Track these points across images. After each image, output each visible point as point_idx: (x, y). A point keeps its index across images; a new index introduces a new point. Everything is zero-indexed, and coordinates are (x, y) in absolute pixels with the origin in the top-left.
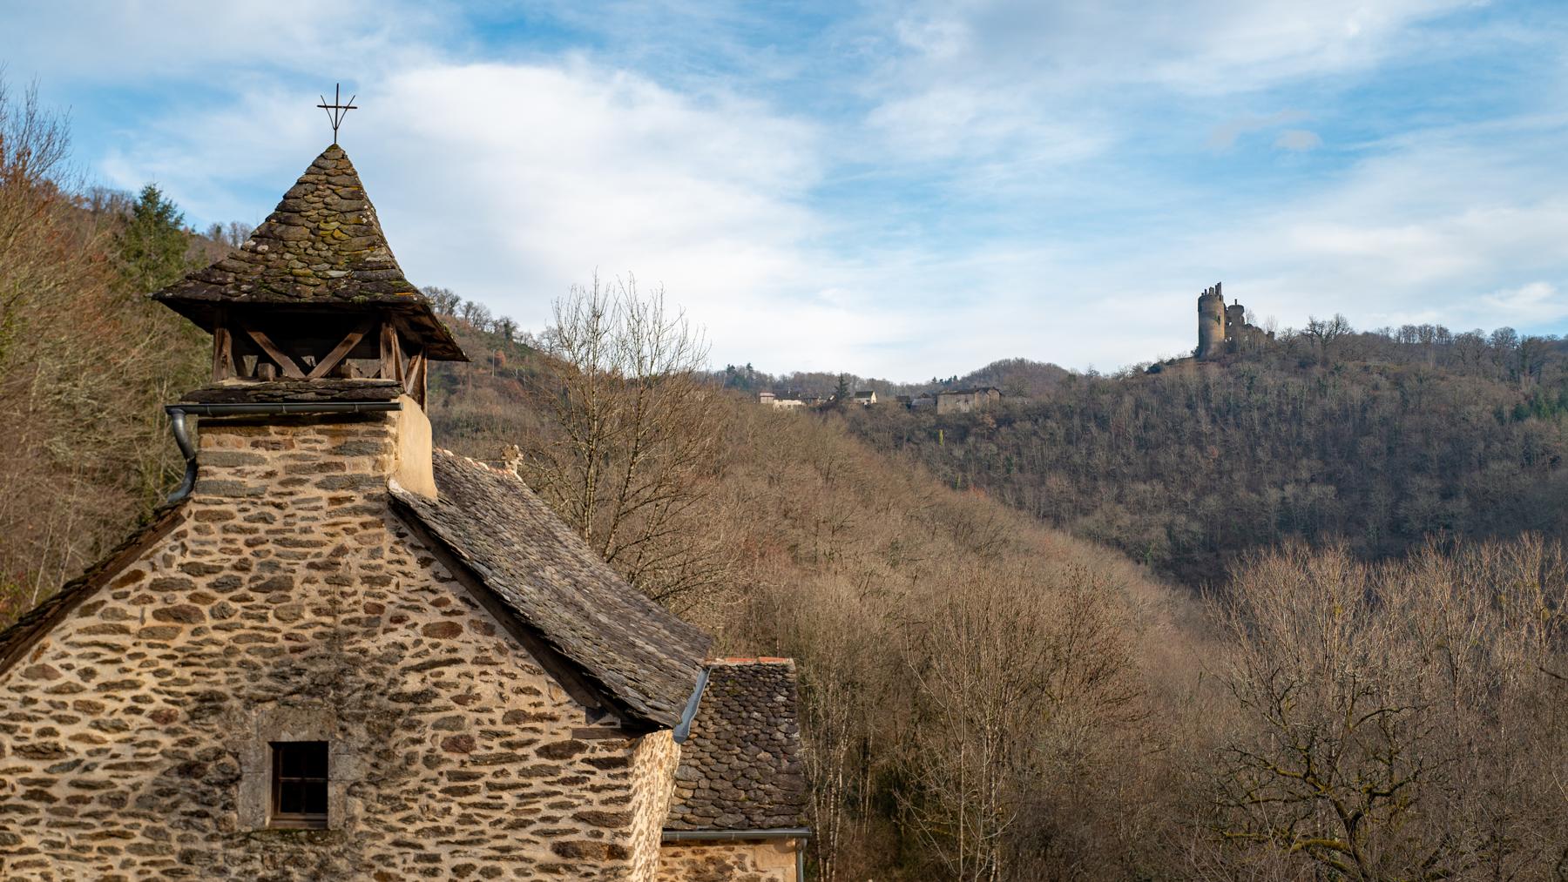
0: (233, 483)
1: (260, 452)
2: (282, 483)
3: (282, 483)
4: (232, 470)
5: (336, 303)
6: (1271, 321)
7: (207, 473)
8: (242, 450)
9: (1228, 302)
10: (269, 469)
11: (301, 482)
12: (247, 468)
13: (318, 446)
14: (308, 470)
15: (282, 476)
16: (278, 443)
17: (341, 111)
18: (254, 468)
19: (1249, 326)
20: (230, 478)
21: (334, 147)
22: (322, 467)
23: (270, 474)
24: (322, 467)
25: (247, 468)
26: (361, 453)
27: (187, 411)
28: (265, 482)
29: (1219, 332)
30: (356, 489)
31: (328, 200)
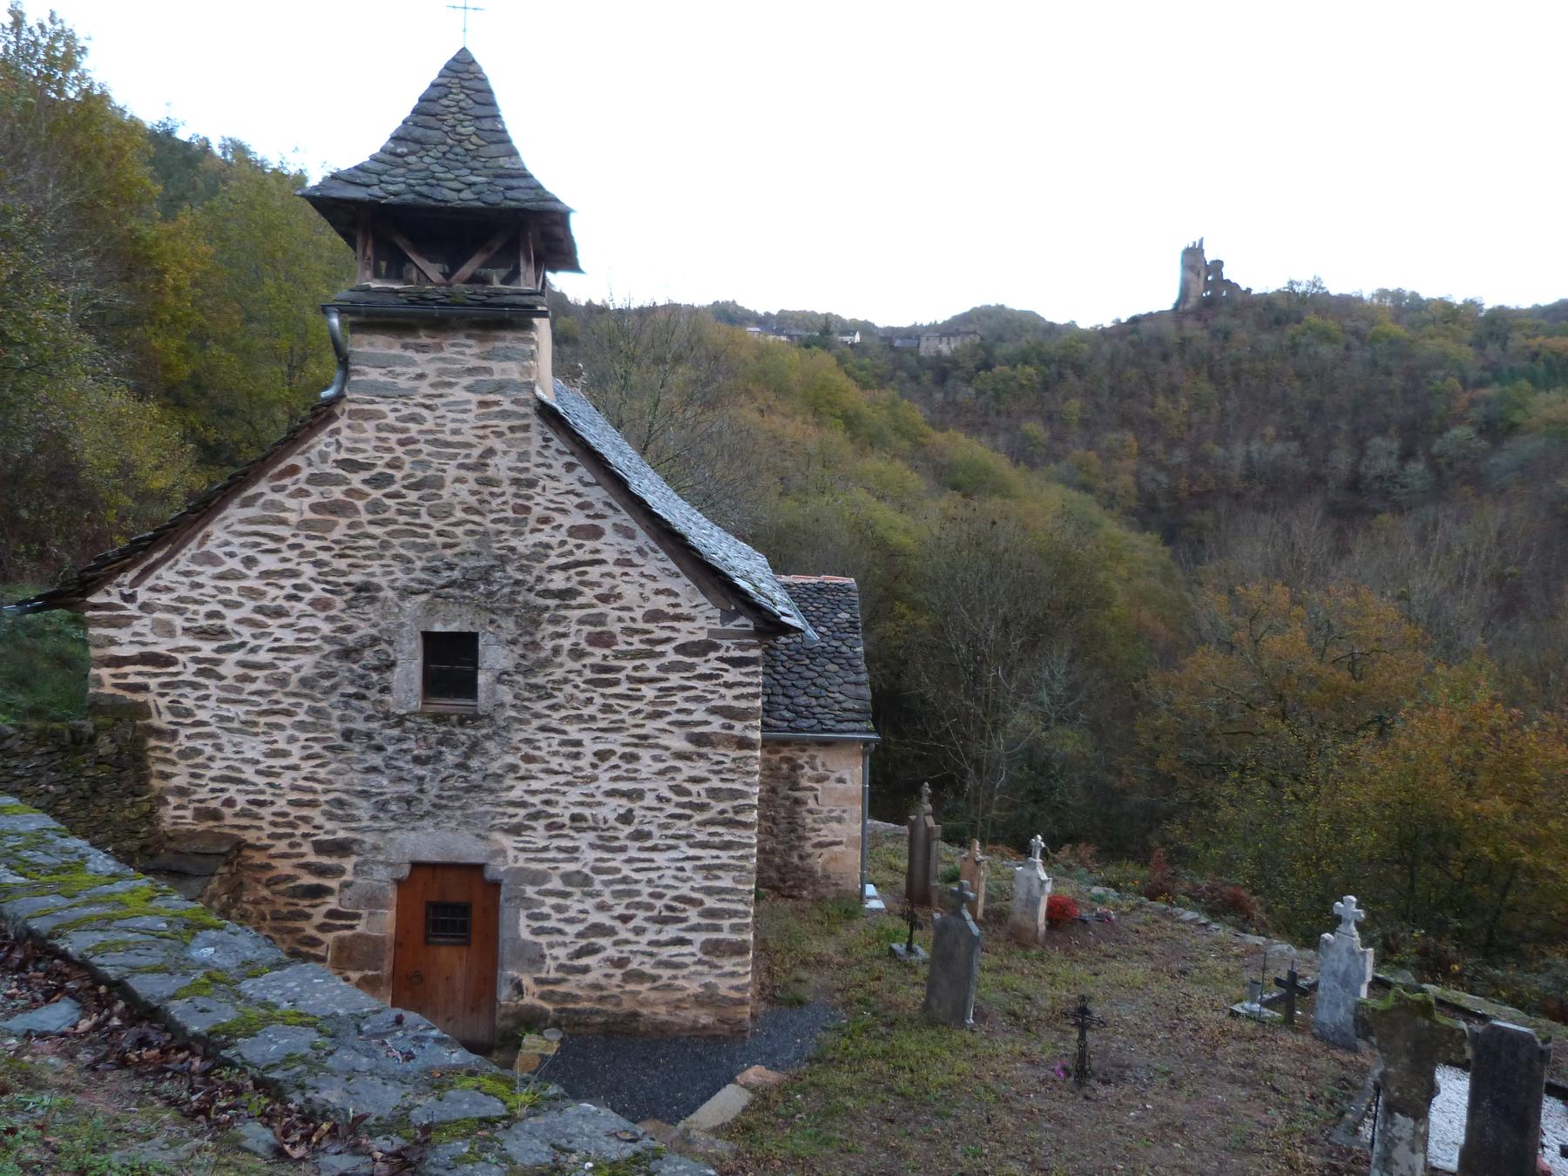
0: (385, 383)
1: (410, 353)
2: (432, 385)
3: (432, 385)
7: (358, 372)
8: (393, 352)
9: (1209, 257)
10: (419, 371)
11: (450, 385)
12: (398, 369)
13: (467, 351)
14: (458, 374)
15: (432, 378)
20: (382, 379)
22: (471, 371)
23: (421, 376)
24: (471, 371)
25: (398, 369)
26: (507, 358)
28: (415, 383)
31: (462, 104)
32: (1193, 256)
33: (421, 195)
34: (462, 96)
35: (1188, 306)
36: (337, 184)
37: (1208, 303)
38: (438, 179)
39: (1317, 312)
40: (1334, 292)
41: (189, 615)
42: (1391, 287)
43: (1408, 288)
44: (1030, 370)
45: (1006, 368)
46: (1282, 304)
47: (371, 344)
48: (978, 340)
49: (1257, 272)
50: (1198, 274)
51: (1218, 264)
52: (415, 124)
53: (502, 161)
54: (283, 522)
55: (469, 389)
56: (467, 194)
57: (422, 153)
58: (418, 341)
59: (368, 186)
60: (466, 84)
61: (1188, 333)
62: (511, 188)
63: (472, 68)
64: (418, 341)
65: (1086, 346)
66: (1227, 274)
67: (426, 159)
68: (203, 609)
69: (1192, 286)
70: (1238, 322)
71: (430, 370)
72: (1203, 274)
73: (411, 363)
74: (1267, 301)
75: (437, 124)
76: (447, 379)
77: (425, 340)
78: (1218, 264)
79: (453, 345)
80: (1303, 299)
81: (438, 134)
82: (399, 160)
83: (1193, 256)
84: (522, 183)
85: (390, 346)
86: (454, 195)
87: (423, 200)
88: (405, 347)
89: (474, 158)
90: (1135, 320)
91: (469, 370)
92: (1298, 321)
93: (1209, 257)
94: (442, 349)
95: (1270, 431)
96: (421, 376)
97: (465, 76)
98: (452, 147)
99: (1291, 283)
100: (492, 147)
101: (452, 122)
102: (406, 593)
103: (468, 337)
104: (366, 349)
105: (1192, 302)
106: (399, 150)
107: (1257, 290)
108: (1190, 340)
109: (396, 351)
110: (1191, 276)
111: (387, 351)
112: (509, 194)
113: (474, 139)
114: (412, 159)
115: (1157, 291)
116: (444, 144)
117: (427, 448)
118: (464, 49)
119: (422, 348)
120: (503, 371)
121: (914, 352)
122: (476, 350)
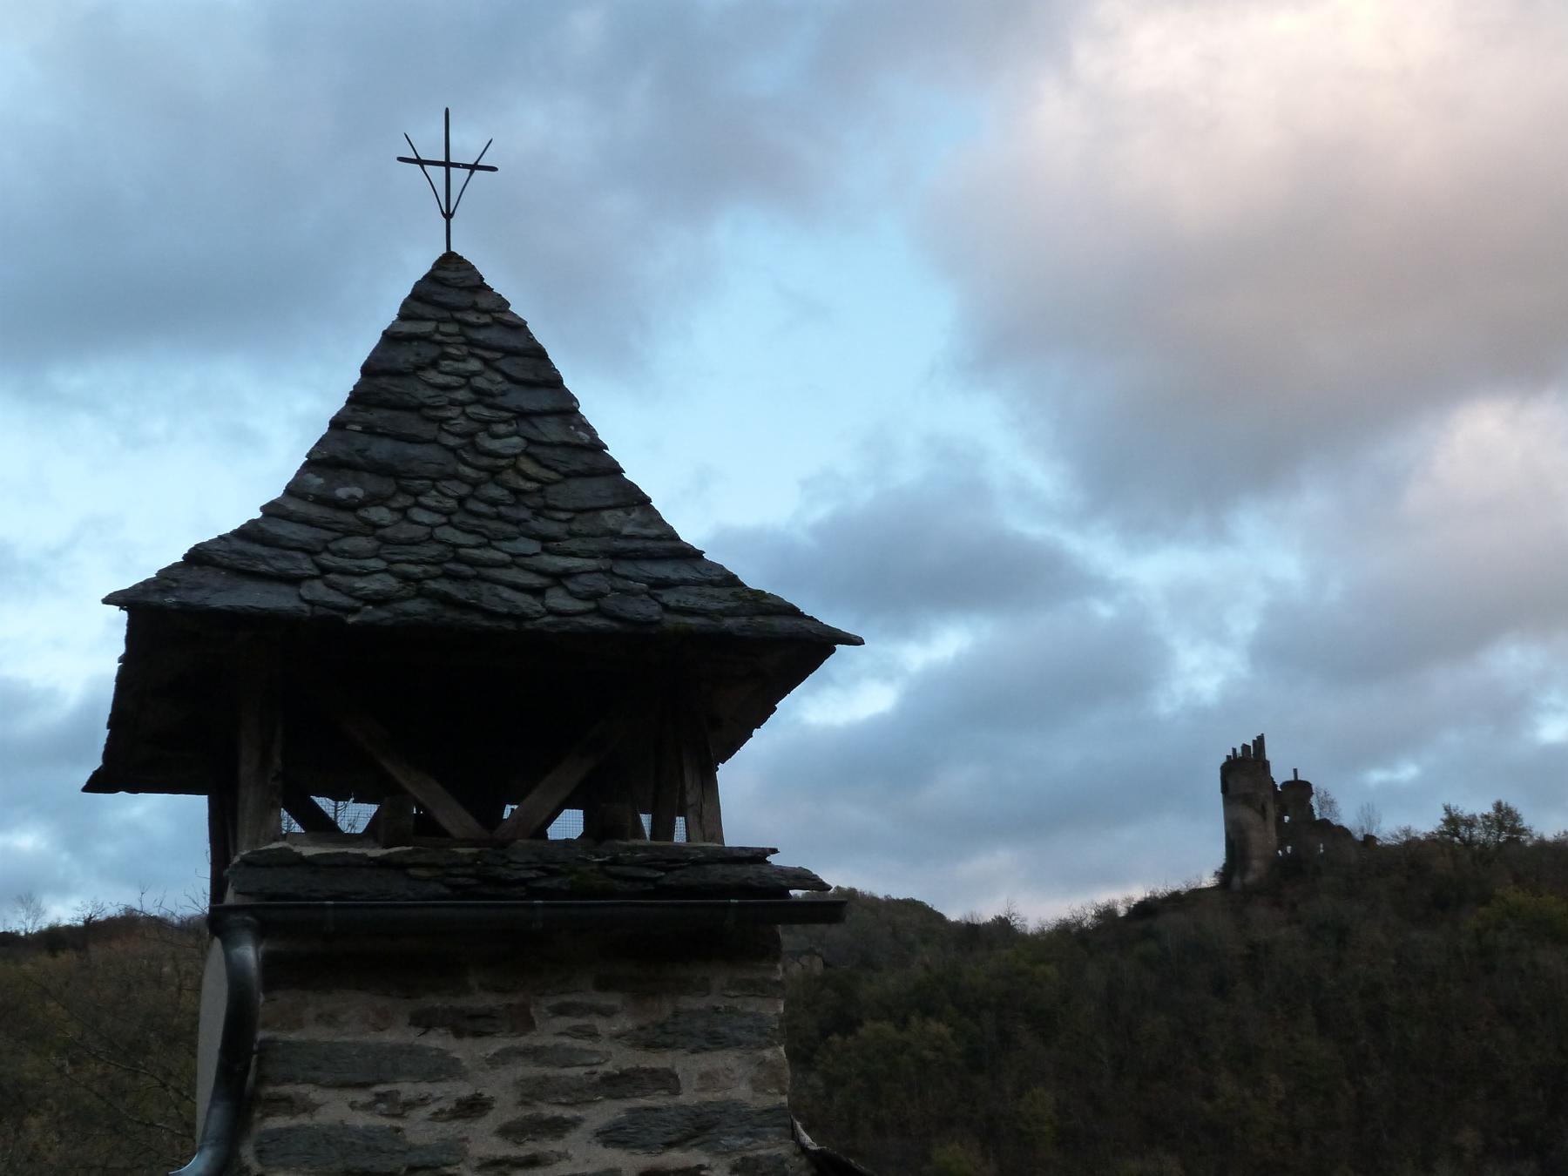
0: (368, 1134)
1: (436, 1040)
2: (505, 1132)
3: (505, 1132)
4: (363, 1097)
5: (596, 633)
6: (1368, 813)
7: (289, 1105)
8: (390, 1037)
9: (1280, 774)
10: (465, 1091)
11: (558, 1127)
12: (407, 1089)
13: (601, 1024)
14: (582, 1094)
15: (507, 1110)
16: (489, 1015)
17: (438, 173)
18: (425, 1088)
19: (1325, 823)
20: (361, 1120)
21: (450, 260)
22: (616, 1084)
23: (474, 1107)
24: (616, 1084)
25: (407, 1089)
26: (716, 1041)
27: (263, 931)
28: (454, 1128)
29: (1264, 840)
30: (710, 1147)
31: (479, 382)
33: (446, 600)
34: (474, 365)
35: (1251, 878)
36: (214, 578)
38: (472, 563)
39: (1518, 880)
40: (1549, 836)
44: (937, 1027)
45: (887, 1028)
47: (329, 1019)
48: (818, 967)
50: (1263, 812)
52: (369, 430)
53: (610, 519)
55: (612, 1137)
56: (558, 599)
57: (402, 501)
58: (463, 1002)
59: (295, 581)
60: (480, 335)
62: (666, 584)
63: (483, 302)
64: (463, 1002)
65: (1051, 970)
67: (419, 515)
69: (1255, 836)
71: (500, 1085)
72: (1272, 811)
73: (444, 1068)
74: (1413, 853)
75: (428, 431)
76: (549, 1111)
77: (486, 1001)
79: (561, 1011)
80: (1483, 855)
81: (433, 453)
82: (346, 517)
84: (686, 572)
85: (383, 1021)
86: (525, 602)
87: (450, 614)
88: (425, 1022)
89: (538, 512)
91: (609, 1080)
92: (1485, 899)
93: (1280, 774)
94: (528, 1025)
95: (1469, 1137)
96: (474, 1107)
97: (471, 317)
98: (475, 485)
100: (575, 484)
101: (462, 424)
103: (603, 985)
104: (316, 1033)
106: (342, 493)
109: (398, 1035)
111: (371, 1038)
112: (670, 598)
113: (527, 466)
114: (378, 514)
116: (455, 476)
118: (450, 260)
119: (471, 1025)
120: (708, 1078)
122: (625, 1023)
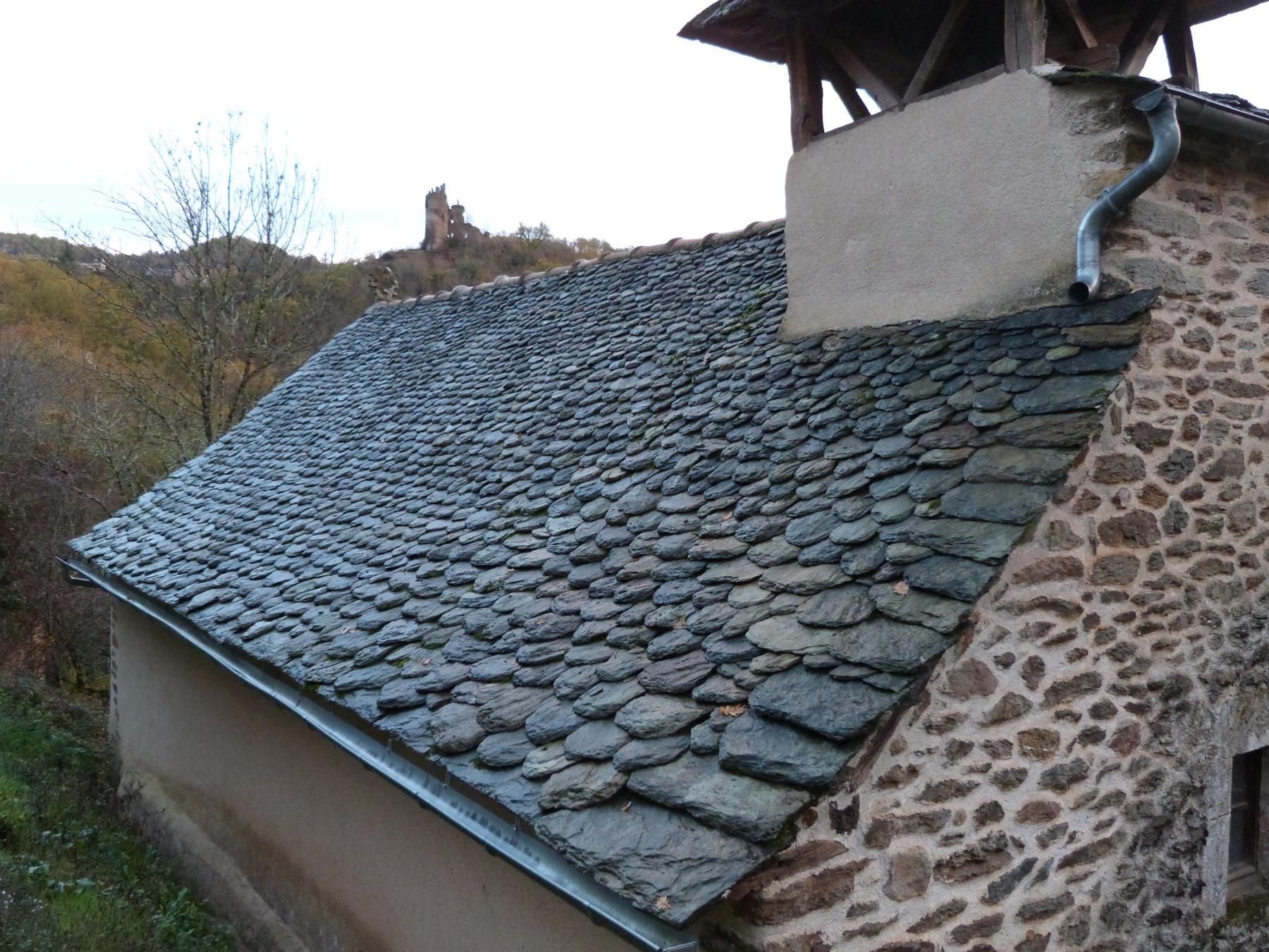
9: (451, 202)
32: (436, 200)
35: (435, 246)
37: (453, 244)
41: (949, 829)
42: (588, 237)
43: (601, 238)
46: (516, 247)
49: (494, 217)
51: (459, 209)
54: (1074, 570)
61: (439, 271)
66: (467, 217)
68: (969, 805)
70: (481, 263)
72: (446, 217)
77: (1205, 189)
78: (459, 209)
83: (436, 200)
90: (387, 257)
93: (451, 202)
99: (522, 230)
102: (1217, 685)
105: (438, 241)
107: (494, 231)
108: (442, 277)
110: (436, 218)
115: (407, 232)
117: (1220, 398)
121: (167, 282)
